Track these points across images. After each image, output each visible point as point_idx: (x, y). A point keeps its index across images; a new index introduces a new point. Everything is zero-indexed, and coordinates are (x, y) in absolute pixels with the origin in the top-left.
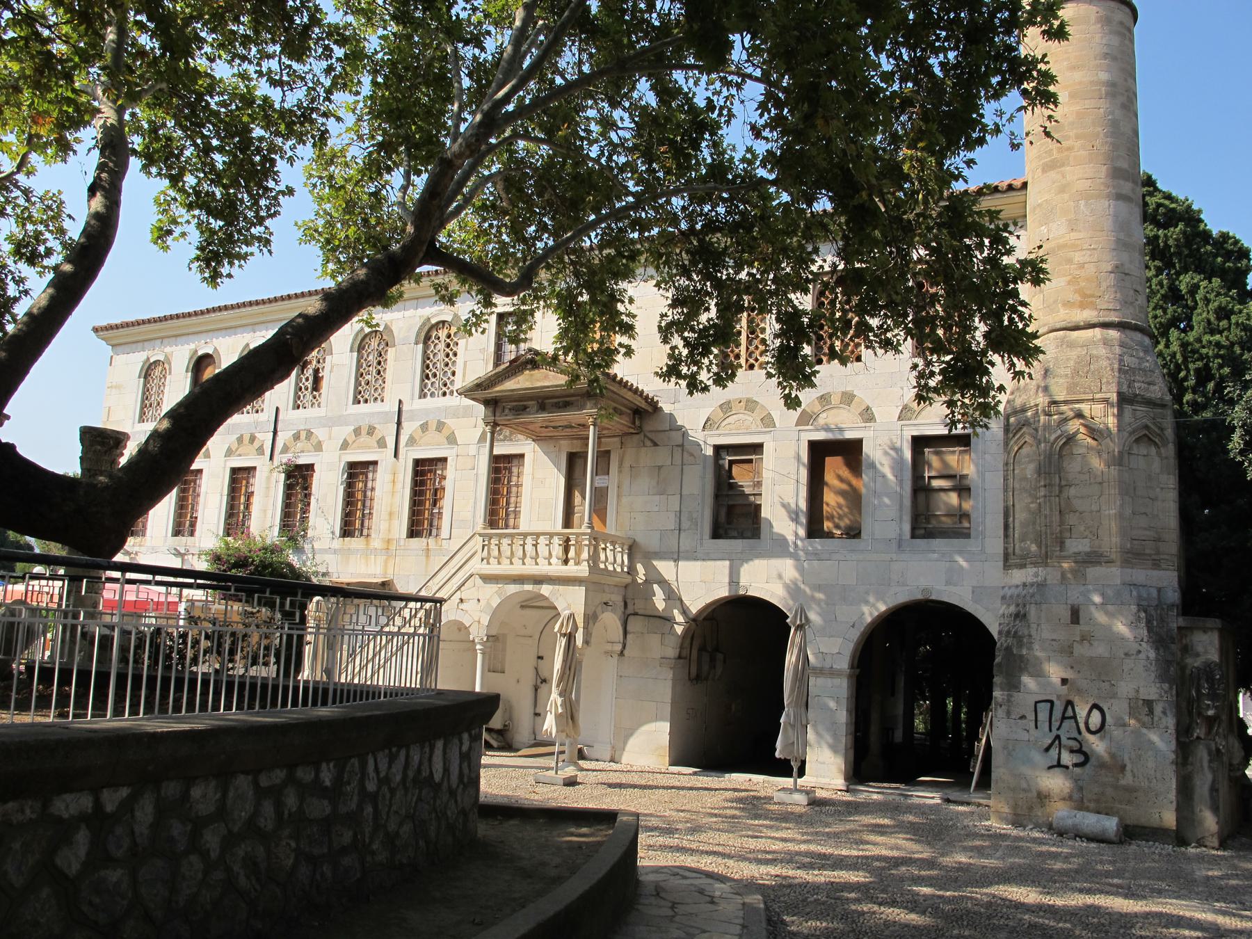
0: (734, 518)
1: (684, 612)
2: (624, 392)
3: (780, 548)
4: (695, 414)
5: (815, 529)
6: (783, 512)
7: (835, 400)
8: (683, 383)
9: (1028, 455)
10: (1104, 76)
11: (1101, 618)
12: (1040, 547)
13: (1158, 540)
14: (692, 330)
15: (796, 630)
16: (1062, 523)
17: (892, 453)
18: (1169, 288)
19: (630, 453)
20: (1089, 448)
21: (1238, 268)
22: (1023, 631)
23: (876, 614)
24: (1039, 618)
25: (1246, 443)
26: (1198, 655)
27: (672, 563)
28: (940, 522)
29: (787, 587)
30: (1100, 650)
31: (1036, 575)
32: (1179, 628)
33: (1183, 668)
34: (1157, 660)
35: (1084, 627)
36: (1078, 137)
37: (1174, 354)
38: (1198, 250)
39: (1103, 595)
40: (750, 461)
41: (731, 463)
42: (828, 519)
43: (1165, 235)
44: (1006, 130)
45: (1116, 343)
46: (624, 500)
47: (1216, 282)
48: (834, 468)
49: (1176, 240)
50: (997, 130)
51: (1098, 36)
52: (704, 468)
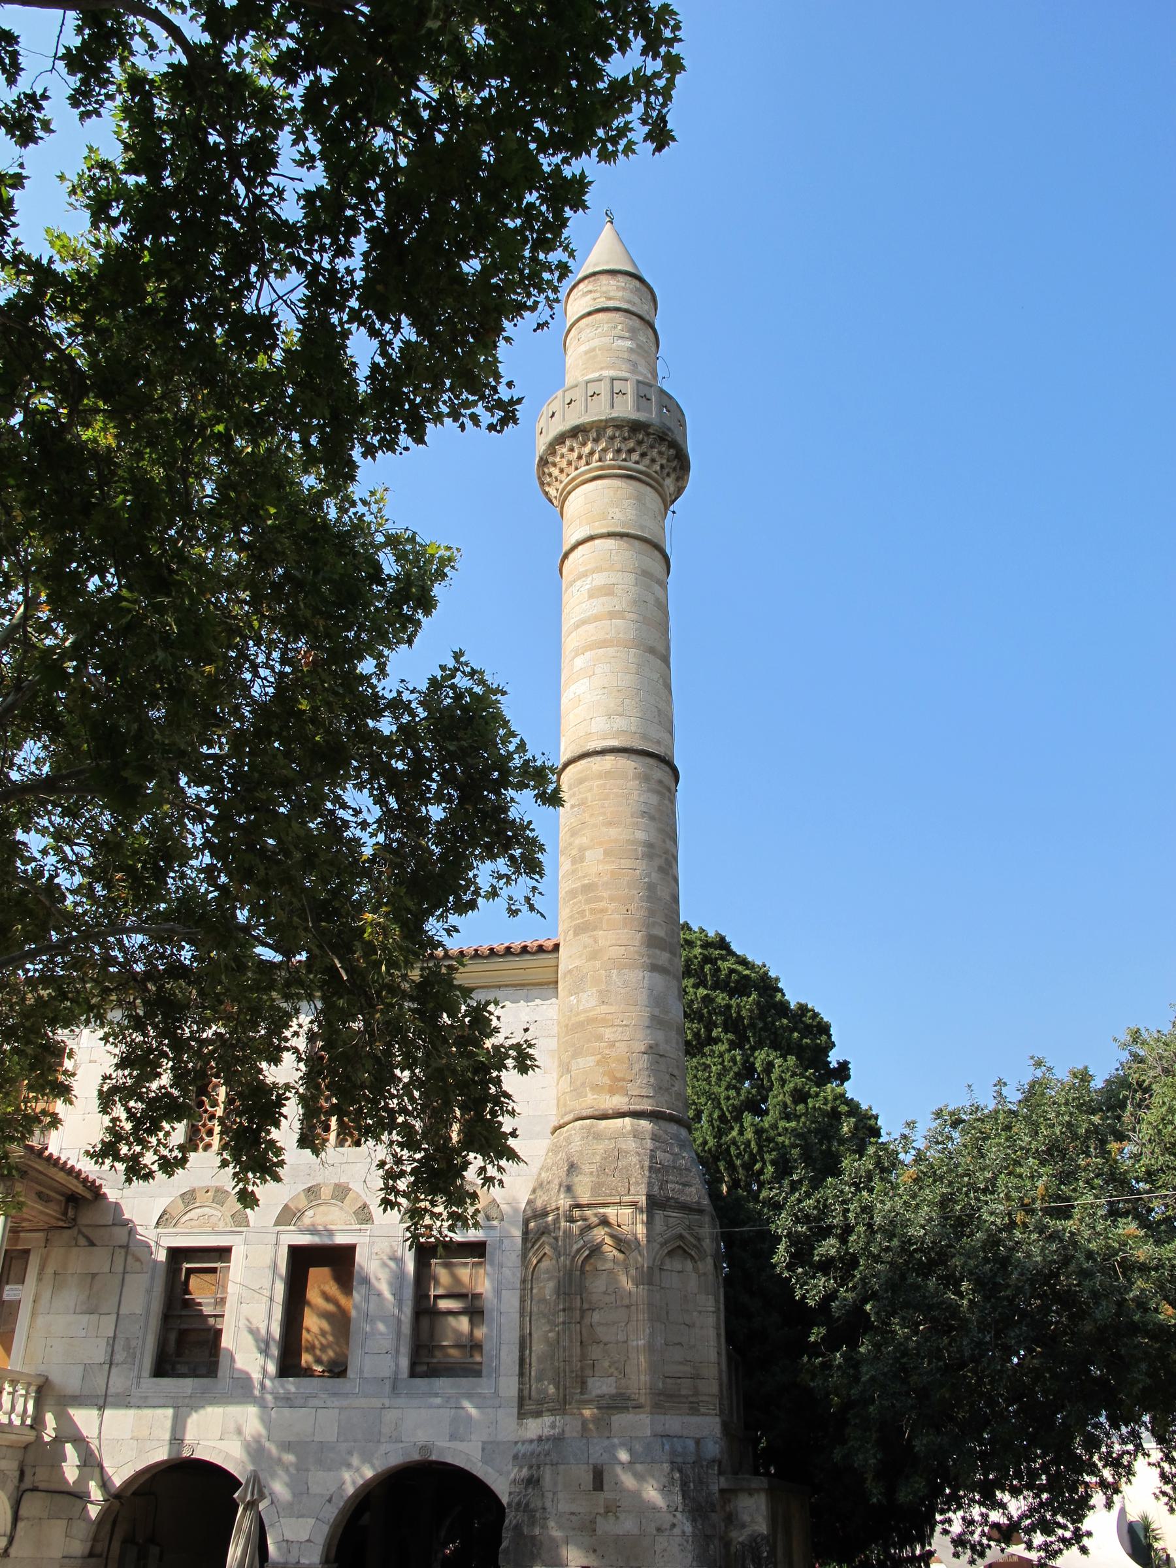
0: (185, 1348)
1: (104, 1484)
2: (52, 1172)
3: (242, 1390)
4: (157, 1209)
5: (289, 1365)
6: (249, 1340)
7: (326, 1193)
8: (121, 1167)
9: (547, 1271)
10: (641, 835)
11: (628, 1481)
12: (558, 1388)
13: (696, 1377)
14: (140, 1098)
15: (245, 1510)
16: (583, 1357)
17: (392, 1264)
18: (744, 1064)
19: (57, 1253)
20: (614, 1260)
21: (817, 1045)
22: (536, 1503)
23: (361, 1482)
24: (555, 1484)
25: (792, 1256)
26: (743, 1526)
27: (94, 1413)
28: (448, 1355)
29: (247, 1447)
30: (627, 1525)
31: (553, 1426)
32: (722, 1491)
33: (727, 1544)
34: (694, 1535)
35: (607, 1495)
36: (612, 899)
37: (749, 1141)
38: (773, 1023)
39: (631, 1451)
40: (213, 1271)
41: (190, 1271)
42: (307, 1350)
43: (738, 1005)
44: (505, 893)
45: (648, 1136)
46: (40, 1321)
47: (792, 1060)
48: (320, 1282)
49: (751, 1011)
50: (494, 893)
51: (636, 792)
52: (152, 1278)
